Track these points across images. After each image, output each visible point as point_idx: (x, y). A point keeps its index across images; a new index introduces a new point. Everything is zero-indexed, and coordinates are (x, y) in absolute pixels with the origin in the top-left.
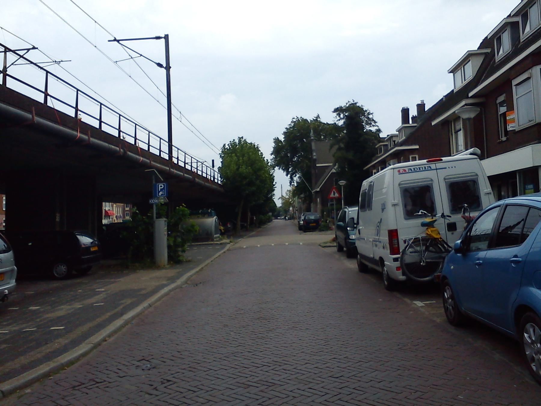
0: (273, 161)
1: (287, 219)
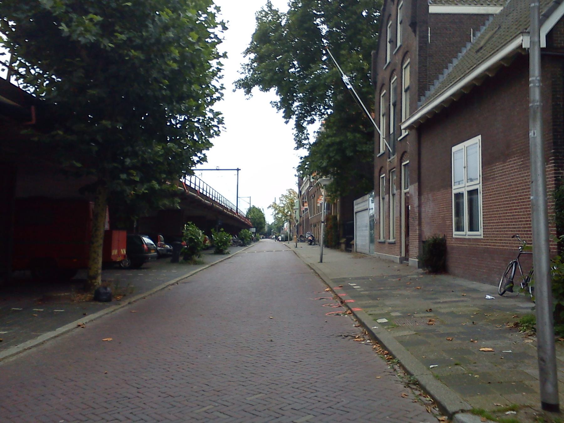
1: (280, 239)
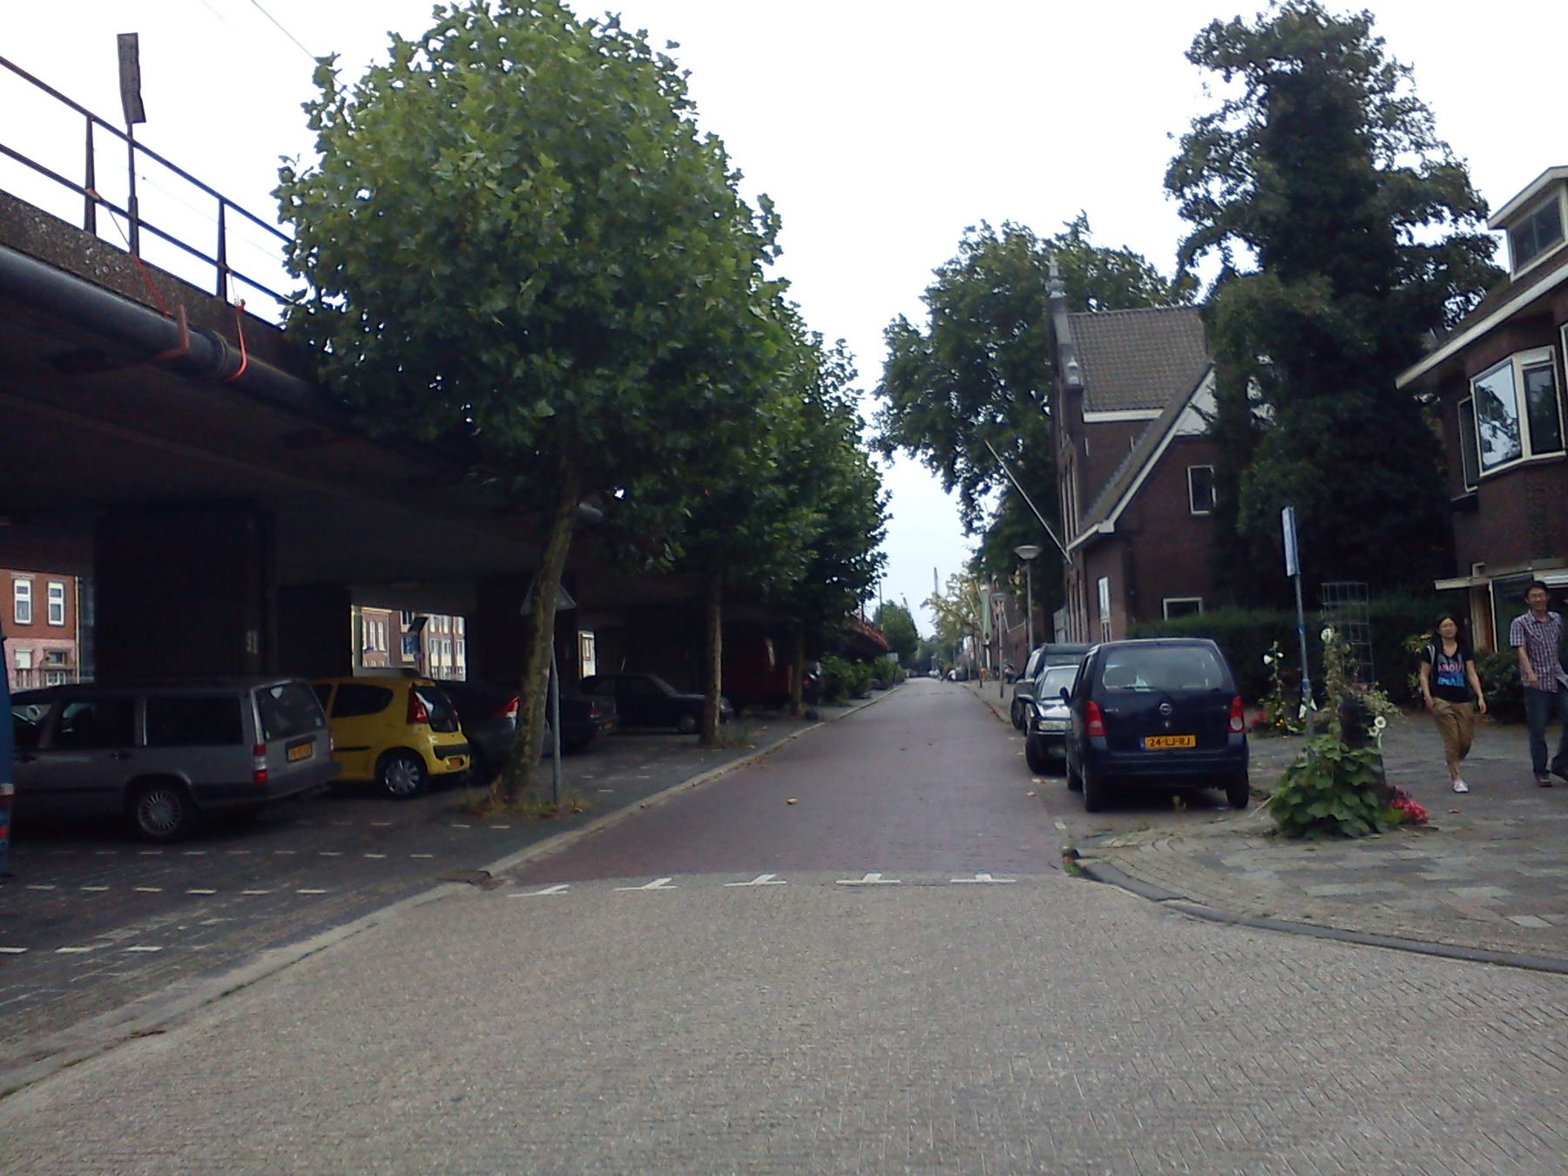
0: (885, 422)
1: (954, 677)
